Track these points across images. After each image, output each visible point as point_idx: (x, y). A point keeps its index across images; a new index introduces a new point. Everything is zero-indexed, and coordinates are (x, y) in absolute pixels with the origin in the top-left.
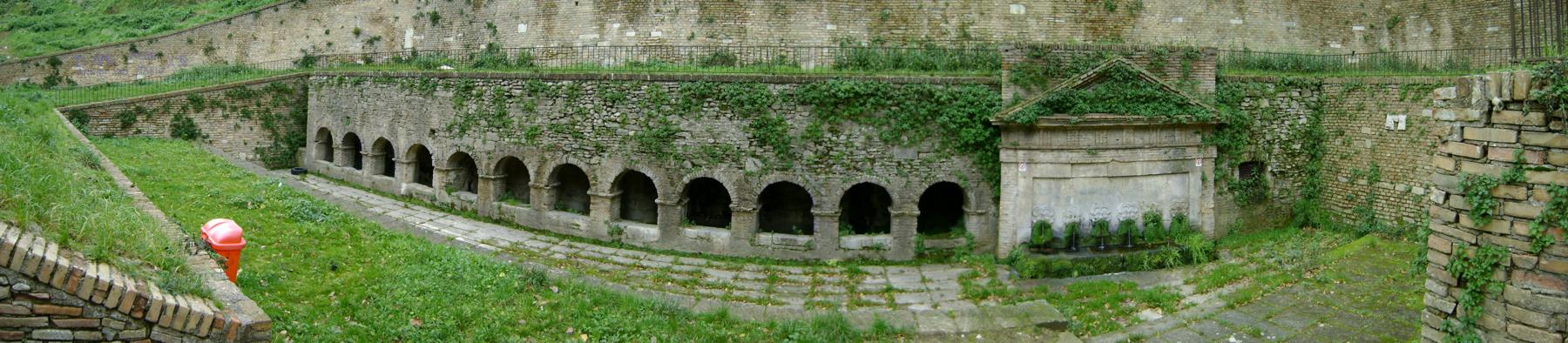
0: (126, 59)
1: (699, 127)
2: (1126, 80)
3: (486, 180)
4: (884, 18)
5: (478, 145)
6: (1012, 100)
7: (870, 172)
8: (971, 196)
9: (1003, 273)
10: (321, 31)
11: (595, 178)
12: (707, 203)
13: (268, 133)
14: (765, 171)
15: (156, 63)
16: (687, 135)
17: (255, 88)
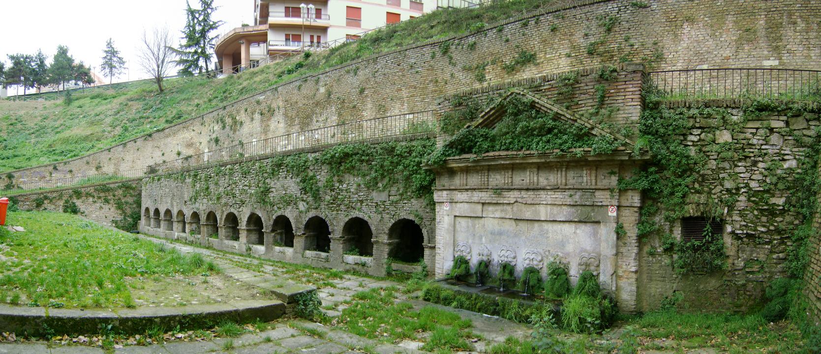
0: (51, 174)
1: (279, 185)
7: (360, 210)
13: (120, 212)
14: (308, 210)
15: (69, 176)
17: (112, 186)
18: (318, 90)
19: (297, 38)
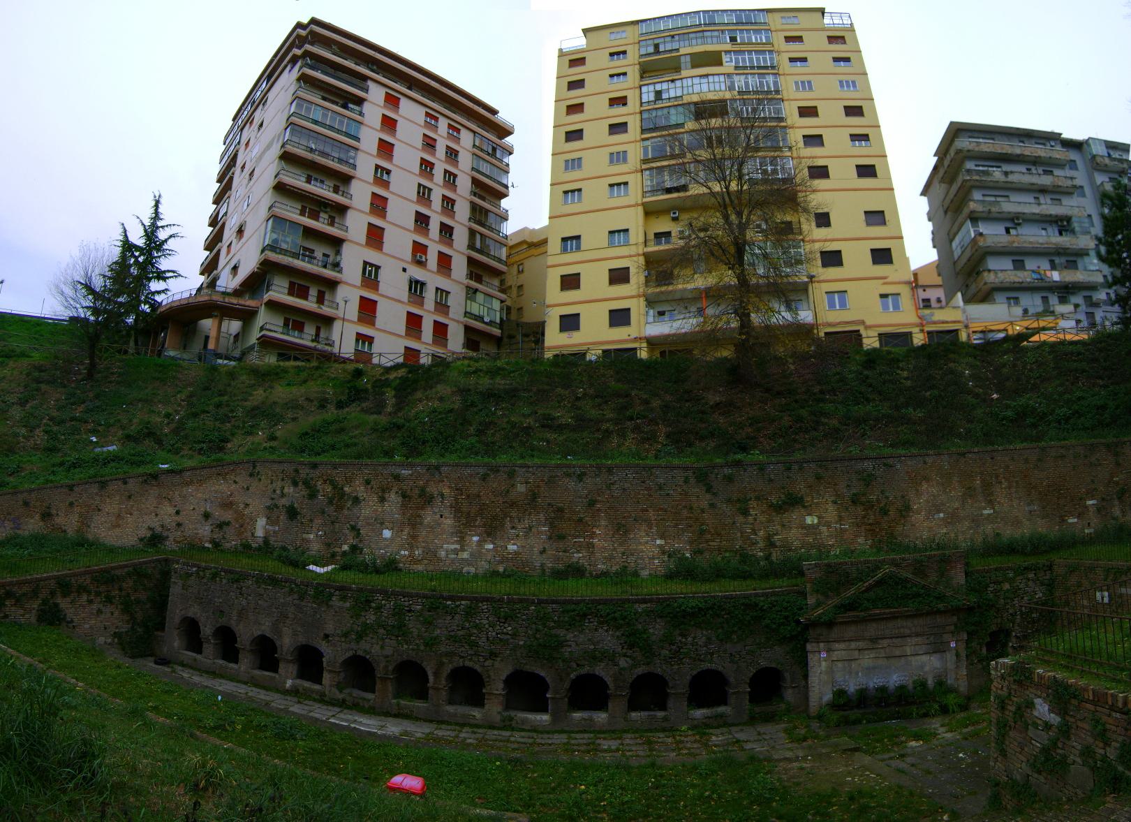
1: (582, 638)
2: (897, 584)
3: (384, 679)
4: (702, 533)
5: (376, 649)
6: (816, 606)
8: (787, 675)
9: (815, 725)
10: (171, 510)
11: (489, 677)
12: (589, 693)
16: (573, 644)
17: (118, 572)
18: (513, 485)
19: (299, 327)
